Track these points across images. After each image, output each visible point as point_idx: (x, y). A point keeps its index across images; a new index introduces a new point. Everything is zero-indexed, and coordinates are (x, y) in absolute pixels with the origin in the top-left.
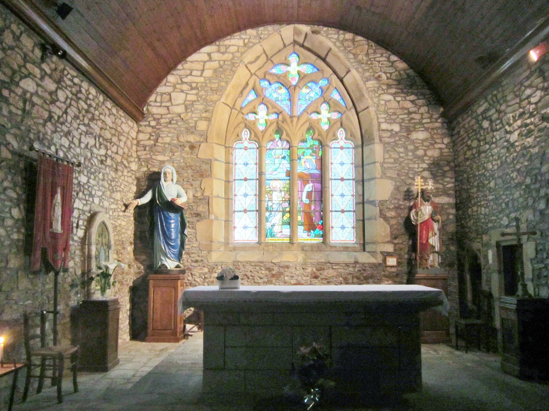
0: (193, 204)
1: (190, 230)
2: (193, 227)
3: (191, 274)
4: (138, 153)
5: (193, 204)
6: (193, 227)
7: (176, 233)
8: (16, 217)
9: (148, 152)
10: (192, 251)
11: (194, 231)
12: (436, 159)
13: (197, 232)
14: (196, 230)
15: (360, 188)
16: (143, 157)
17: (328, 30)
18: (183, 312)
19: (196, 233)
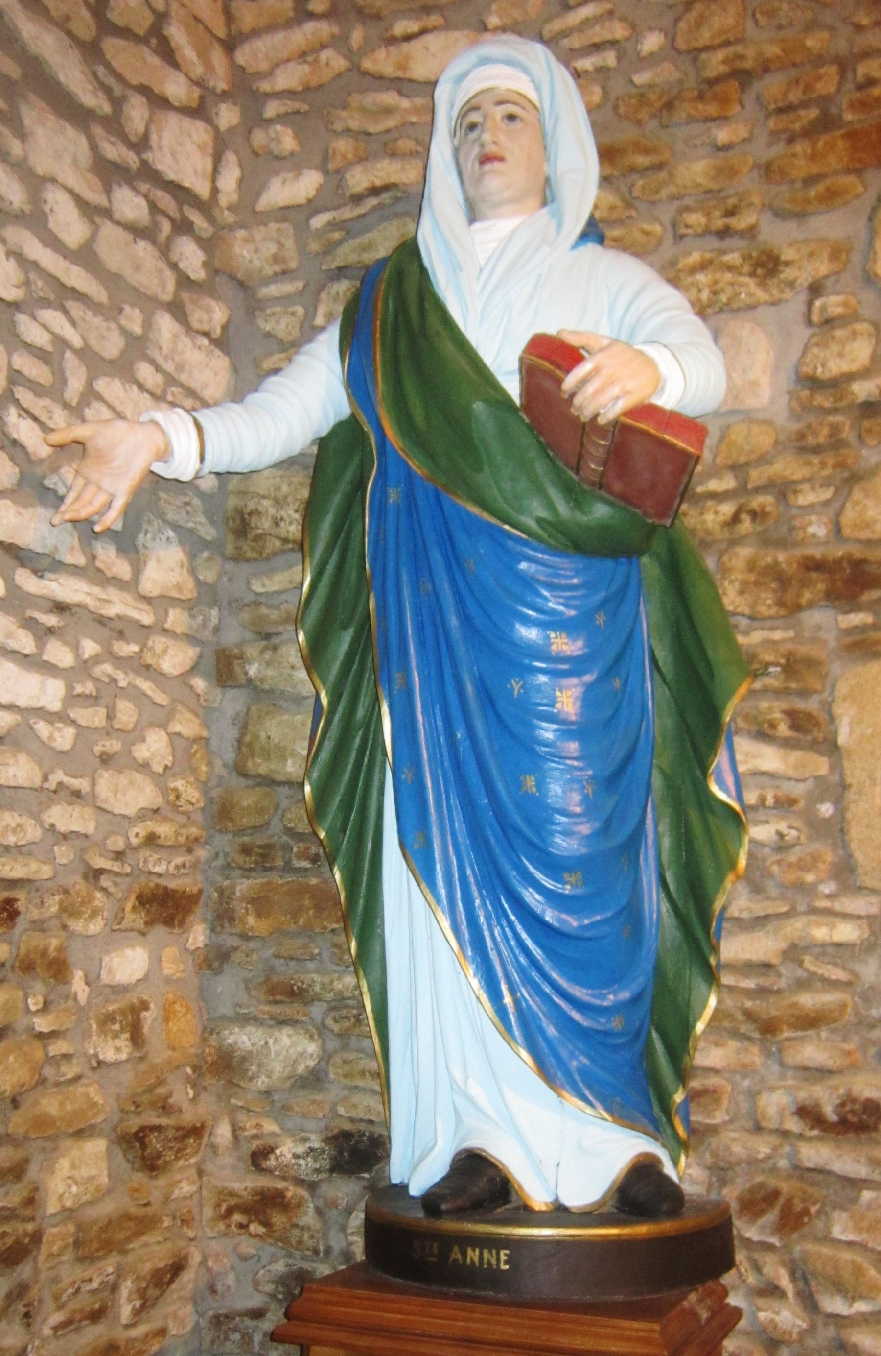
0: (787, 467)
1: (768, 758)
2: (800, 722)
3: (800, 1272)
4: (242, 56)
5: (787, 467)
6: (800, 722)
7: (613, 780)
8: (845, 1215)
9: (324, 29)
10: (808, 1000)
11: (821, 765)
12: (124, 1146)
13: (854, 773)
14: (830, 747)
15: (865, 892)
16: (288, 78)
17: (792, 474)
18: (61, 429)
19: (837, 790)
